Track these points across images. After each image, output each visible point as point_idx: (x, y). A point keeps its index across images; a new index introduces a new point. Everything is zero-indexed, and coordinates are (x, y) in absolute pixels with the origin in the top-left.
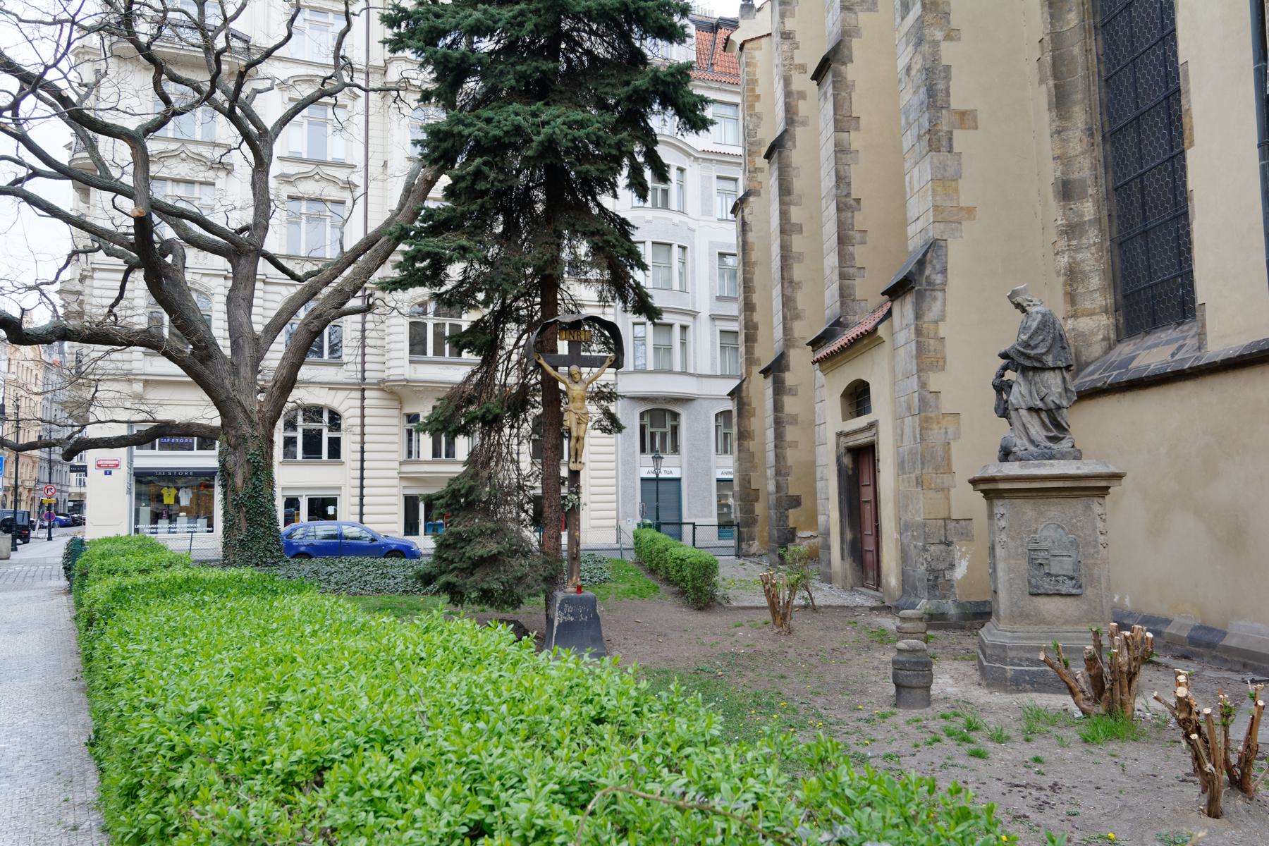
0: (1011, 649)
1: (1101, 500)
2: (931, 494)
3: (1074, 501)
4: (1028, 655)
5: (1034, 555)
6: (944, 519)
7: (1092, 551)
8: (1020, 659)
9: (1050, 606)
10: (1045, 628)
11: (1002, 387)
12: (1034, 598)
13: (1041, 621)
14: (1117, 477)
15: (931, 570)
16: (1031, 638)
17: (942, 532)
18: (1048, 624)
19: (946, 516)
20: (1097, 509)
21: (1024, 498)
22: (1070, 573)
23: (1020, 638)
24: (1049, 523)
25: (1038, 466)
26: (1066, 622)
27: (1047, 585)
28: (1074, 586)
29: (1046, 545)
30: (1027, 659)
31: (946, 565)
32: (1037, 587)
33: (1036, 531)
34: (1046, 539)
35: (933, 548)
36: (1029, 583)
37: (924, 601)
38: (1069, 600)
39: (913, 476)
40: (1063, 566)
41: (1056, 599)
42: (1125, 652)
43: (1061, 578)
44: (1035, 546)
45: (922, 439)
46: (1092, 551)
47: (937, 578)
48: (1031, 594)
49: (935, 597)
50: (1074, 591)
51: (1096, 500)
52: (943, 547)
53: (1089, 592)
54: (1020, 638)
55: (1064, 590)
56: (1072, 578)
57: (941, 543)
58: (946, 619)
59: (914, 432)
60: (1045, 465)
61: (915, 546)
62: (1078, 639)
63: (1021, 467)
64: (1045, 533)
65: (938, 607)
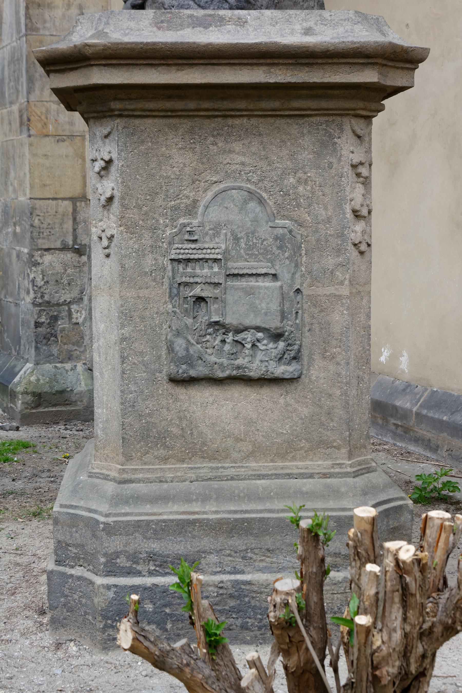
0: (110, 530)
1: (359, 125)
2: (48, 145)
3: (293, 128)
4: (155, 546)
5: (184, 273)
6: (74, 200)
7: (330, 261)
8: (134, 557)
9: (218, 411)
10: (205, 467)
11: (370, 212)
12: (182, 393)
13: (194, 448)
14: (406, 59)
15: (43, 304)
16: (164, 499)
17: (69, 225)
18: (214, 456)
19: (77, 191)
20: (349, 150)
21: (168, 114)
22: (274, 323)
23: (137, 499)
24: (228, 187)
25: (205, 24)
26: (257, 452)
27: (216, 357)
28: (274, 360)
29: (216, 246)
30: (152, 557)
31: (75, 293)
32: (188, 360)
33: (191, 210)
34: (217, 229)
35: (48, 258)
36: (170, 349)
37: (29, 365)
38: (267, 394)
39: (15, 108)
40: (253, 303)
41: (237, 392)
42: (396, 613)
43: (248, 336)
44: (188, 250)
45: (31, 28)
46: (330, 261)
47: (55, 319)
48: (175, 381)
49: (50, 358)
50: (280, 370)
51: (349, 124)
52: (69, 256)
53: (318, 372)
54: (137, 499)
55: (255, 369)
56: (277, 336)
57: (64, 248)
58: (67, 402)
59: (17, 12)
60: (222, 21)
61: (18, 256)
62: (282, 494)
63: (158, 25)
64: (215, 214)
65: (54, 379)
